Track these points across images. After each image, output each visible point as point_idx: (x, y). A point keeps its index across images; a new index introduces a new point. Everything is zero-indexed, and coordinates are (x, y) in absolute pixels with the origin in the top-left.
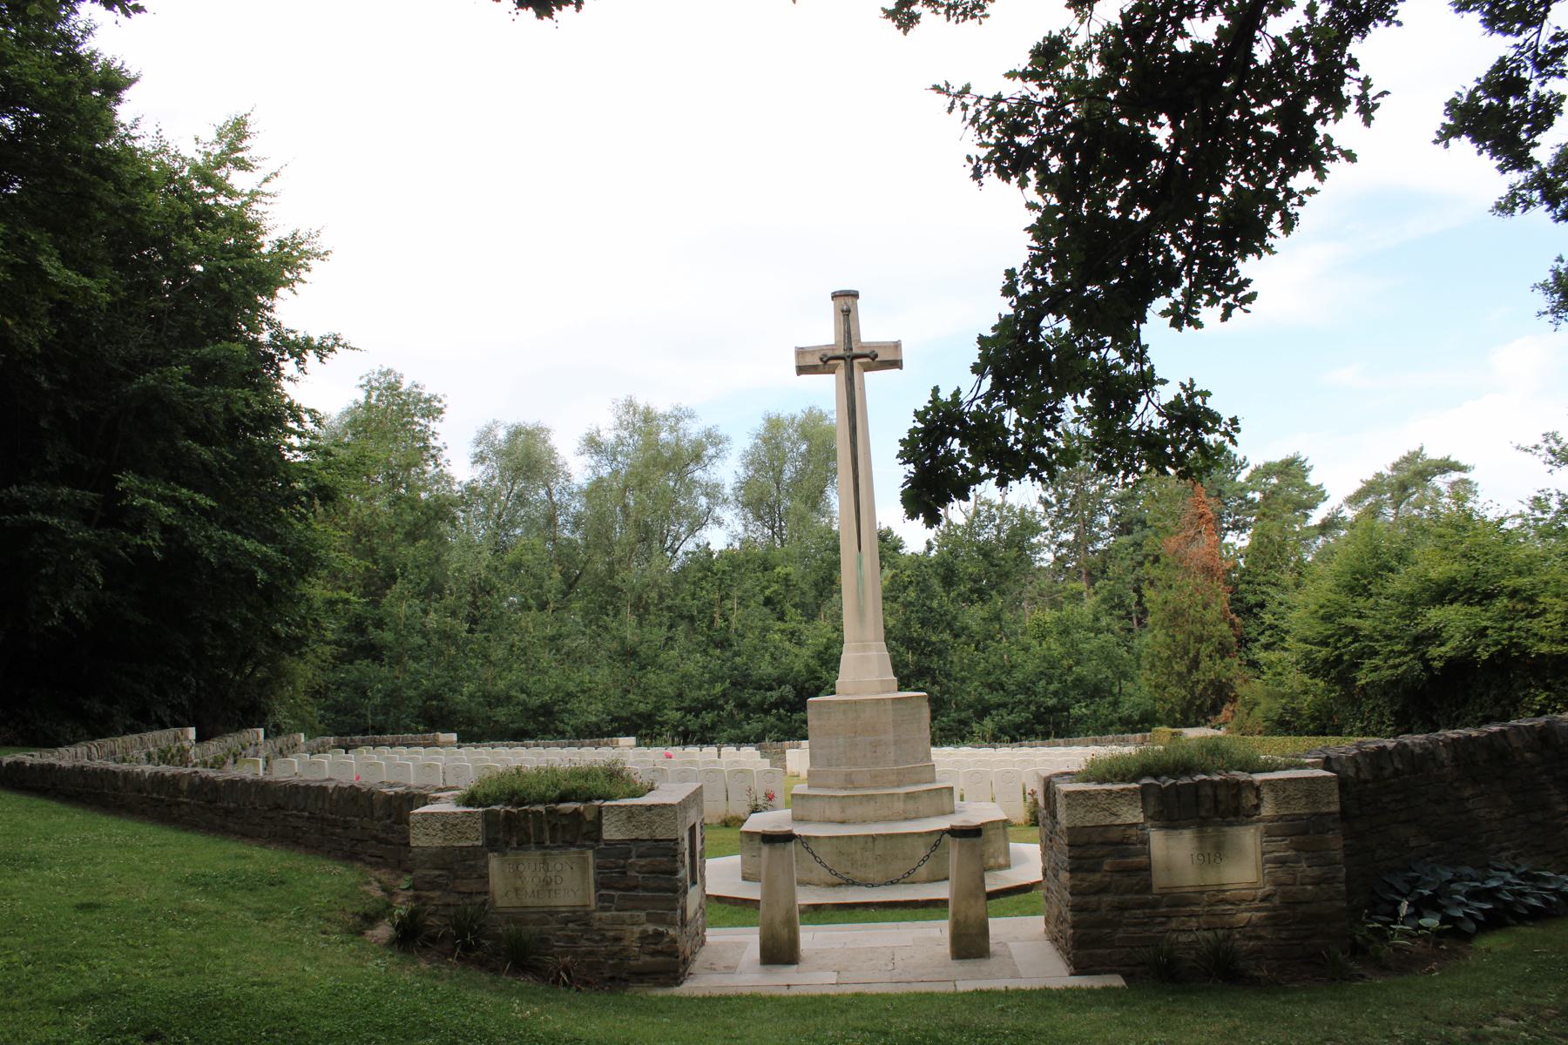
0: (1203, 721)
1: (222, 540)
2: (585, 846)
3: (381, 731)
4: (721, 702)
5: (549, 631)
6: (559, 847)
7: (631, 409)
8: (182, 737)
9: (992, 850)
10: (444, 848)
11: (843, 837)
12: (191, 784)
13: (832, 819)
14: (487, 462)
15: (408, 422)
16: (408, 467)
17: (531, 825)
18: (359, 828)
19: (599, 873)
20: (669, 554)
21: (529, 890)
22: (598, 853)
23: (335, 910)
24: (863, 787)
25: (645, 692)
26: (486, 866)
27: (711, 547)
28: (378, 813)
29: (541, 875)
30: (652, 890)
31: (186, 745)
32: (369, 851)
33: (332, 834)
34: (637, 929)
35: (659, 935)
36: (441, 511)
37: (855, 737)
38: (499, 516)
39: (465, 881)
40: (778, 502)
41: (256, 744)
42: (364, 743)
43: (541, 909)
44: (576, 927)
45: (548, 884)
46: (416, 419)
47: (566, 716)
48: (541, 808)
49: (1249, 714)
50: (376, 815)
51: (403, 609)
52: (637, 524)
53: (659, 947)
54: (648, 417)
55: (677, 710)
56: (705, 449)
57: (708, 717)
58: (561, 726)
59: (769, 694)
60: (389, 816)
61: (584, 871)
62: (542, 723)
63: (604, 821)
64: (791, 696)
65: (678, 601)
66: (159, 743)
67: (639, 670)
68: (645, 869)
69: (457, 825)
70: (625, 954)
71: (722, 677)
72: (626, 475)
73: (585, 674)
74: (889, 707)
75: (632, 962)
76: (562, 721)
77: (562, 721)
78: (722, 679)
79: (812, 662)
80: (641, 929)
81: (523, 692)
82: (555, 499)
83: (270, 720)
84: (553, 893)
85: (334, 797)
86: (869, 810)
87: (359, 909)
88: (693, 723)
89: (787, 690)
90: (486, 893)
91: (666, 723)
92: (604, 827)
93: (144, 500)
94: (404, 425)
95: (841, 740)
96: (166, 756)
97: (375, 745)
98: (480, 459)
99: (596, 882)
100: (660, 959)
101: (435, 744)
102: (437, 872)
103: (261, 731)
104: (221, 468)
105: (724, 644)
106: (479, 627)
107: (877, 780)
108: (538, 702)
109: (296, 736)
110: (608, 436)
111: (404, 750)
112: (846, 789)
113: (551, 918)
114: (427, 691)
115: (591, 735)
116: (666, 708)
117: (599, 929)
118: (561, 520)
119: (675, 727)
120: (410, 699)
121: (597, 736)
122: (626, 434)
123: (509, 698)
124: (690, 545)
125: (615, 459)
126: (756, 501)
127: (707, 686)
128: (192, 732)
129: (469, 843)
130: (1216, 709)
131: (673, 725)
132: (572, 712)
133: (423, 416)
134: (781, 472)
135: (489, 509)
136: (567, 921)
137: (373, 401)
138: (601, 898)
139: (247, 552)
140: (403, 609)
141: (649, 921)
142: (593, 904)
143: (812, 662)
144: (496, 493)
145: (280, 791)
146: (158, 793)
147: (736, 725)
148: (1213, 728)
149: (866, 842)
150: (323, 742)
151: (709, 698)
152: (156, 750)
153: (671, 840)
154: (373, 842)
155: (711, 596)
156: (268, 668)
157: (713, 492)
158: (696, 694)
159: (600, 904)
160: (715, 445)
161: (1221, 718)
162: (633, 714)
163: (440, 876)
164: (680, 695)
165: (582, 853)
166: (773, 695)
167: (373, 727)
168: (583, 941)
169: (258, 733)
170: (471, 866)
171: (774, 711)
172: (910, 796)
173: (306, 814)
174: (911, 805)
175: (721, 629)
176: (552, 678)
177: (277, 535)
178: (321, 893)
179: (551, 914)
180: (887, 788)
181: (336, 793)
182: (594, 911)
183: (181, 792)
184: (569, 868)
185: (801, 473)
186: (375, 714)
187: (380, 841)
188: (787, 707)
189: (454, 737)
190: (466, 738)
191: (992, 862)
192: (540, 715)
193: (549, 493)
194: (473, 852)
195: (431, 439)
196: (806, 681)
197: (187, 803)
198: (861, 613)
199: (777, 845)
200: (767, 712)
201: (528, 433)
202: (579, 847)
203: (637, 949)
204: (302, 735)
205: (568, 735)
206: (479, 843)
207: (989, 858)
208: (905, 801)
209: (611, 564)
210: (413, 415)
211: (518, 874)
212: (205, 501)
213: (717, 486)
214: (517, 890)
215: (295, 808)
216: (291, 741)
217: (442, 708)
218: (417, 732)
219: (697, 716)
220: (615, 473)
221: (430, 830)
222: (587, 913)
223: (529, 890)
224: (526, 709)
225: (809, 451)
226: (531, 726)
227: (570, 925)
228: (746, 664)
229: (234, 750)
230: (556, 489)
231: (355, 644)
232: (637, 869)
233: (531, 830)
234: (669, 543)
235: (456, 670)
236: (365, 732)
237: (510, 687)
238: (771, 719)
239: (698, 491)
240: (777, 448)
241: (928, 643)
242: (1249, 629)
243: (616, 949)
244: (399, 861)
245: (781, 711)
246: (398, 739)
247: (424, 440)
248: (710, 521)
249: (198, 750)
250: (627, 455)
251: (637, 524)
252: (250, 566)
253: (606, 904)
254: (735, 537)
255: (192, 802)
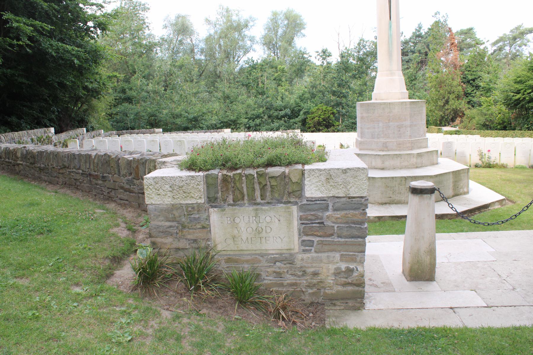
0: (447, 124)
1: (57, 46)
2: (290, 202)
3: (133, 128)
4: (262, 115)
5: (194, 91)
6: (268, 203)
7: (221, 7)
8: (48, 132)
9: (462, 185)
10: (173, 205)
11: (389, 178)
12: (22, 154)
13: (376, 167)
14: (168, 28)
15: (137, 13)
16: (138, 30)
17: (244, 185)
18: (112, 181)
19: (303, 224)
20: (236, 63)
21: (244, 238)
22: (302, 208)
23: (88, 257)
24: (392, 150)
25: (233, 111)
26: (208, 219)
27: (253, 59)
28: (123, 172)
29: (254, 226)
30: (346, 237)
31: (50, 135)
32: (119, 196)
33: (97, 184)
34: (332, 268)
35: (350, 271)
36: (150, 48)
37: (389, 122)
38: (173, 49)
39: (191, 231)
40: (276, 43)
41: (83, 134)
42: (127, 133)
43: (254, 252)
44: (283, 265)
45: (259, 233)
46: (140, 12)
47: (203, 122)
48: (252, 172)
49: (469, 122)
50: (122, 173)
51: (139, 83)
52: (225, 51)
53: (350, 280)
54: (228, 9)
55: (246, 118)
56: (249, 23)
57: (258, 121)
58: (201, 125)
59: (281, 112)
60: (131, 174)
61: (290, 222)
62: (194, 124)
63: (306, 182)
64: (289, 113)
65: (241, 79)
66: (36, 134)
67: (230, 103)
68: (339, 221)
69: (182, 186)
70: (322, 285)
71: (262, 106)
72: (220, 33)
73: (209, 105)
74: (408, 106)
75: (327, 291)
76: (202, 123)
77: (202, 123)
78: (262, 107)
79: (298, 100)
80: (335, 266)
81: (186, 112)
82: (194, 42)
83: (89, 125)
84: (263, 240)
85: (96, 161)
86: (397, 162)
87: (108, 253)
88: (252, 124)
89: (288, 111)
90: (208, 240)
91: (241, 123)
92: (306, 187)
93: (18, 24)
94: (136, 14)
95: (381, 124)
96: (40, 140)
97: (131, 133)
98: (165, 27)
99: (299, 230)
100: (350, 288)
101: (154, 132)
102: (168, 224)
103: (85, 129)
104: (53, 14)
105: (263, 93)
106: (169, 88)
107: (400, 146)
108: (192, 116)
109: (100, 131)
110: (213, 19)
111: (142, 135)
112: (383, 151)
113: (261, 258)
114: (150, 113)
115: (213, 128)
116: (241, 118)
117: (301, 267)
118: (196, 50)
119: (245, 125)
120: (143, 116)
121: (215, 129)
122: (220, 17)
123: (181, 115)
124: (245, 58)
125: (216, 27)
126: (269, 43)
127: (257, 109)
128: (52, 130)
129: (193, 201)
130: (453, 120)
131: (244, 124)
132: (205, 120)
133: (142, 11)
134: (277, 32)
135: (169, 46)
136: (275, 261)
137: (123, 5)
138: (303, 243)
139: (68, 52)
140: (139, 83)
141: (341, 260)
142: (296, 245)
143: (298, 100)
144: (171, 41)
145: (65, 157)
146: (8, 158)
147: (268, 124)
148: (452, 127)
149: (401, 181)
150: (111, 133)
151: (258, 114)
152: (36, 137)
153: (362, 197)
154: (122, 190)
155: (257, 75)
156: (87, 105)
157: (252, 39)
158: (253, 112)
159: (303, 248)
160: (253, 21)
161: (455, 123)
162: (228, 120)
163: (171, 227)
164: (247, 113)
165: (288, 208)
166: (282, 113)
167: (130, 127)
168: (288, 276)
169: (83, 130)
170: (195, 218)
171: (283, 119)
172: (419, 155)
173: (81, 171)
174: (419, 160)
175: (262, 87)
176: (195, 110)
177: (82, 45)
178: (79, 240)
179: (262, 255)
180: (404, 150)
181: (97, 158)
182: (297, 253)
183: (17, 158)
184: (277, 221)
185: (285, 32)
186: (131, 123)
187: (126, 190)
188: (288, 117)
189: (161, 130)
190: (165, 130)
191: (461, 191)
192: (193, 121)
193: (191, 41)
194: (198, 208)
195: (146, 19)
196: (295, 107)
197: (22, 164)
198: (390, 54)
199: (425, 196)
200: (280, 119)
201: (183, 17)
202: (285, 203)
203: (332, 282)
204: (102, 130)
205: (204, 128)
206: (202, 201)
207: (461, 188)
208: (417, 158)
209: (215, 66)
210: (139, 10)
211: (234, 224)
212: (48, 27)
213: (254, 37)
214: (234, 238)
215: (74, 167)
216: (98, 133)
217: (156, 120)
218: (147, 128)
219: (253, 121)
220: (216, 32)
221: (161, 191)
222: (291, 255)
223: (244, 238)
224: (188, 119)
225: (288, 24)
226: (190, 125)
227: (278, 264)
228: (271, 101)
229: (73, 136)
230: (194, 38)
231: (122, 98)
232: (334, 220)
233: (245, 190)
234: (236, 58)
235: (160, 105)
236: (128, 129)
237: (181, 111)
238: (282, 122)
239: (246, 39)
240: (276, 22)
241: (341, 93)
242: (468, 89)
243: (315, 281)
244: (139, 205)
245: (286, 119)
246: (140, 131)
247: (143, 20)
248: (251, 50)
249: (56, 137)
250: (220, 25)
251: (225, 51)
252: (71, 58)
253: (307, 248)
254: (260, 56)
255: (24, 164)
